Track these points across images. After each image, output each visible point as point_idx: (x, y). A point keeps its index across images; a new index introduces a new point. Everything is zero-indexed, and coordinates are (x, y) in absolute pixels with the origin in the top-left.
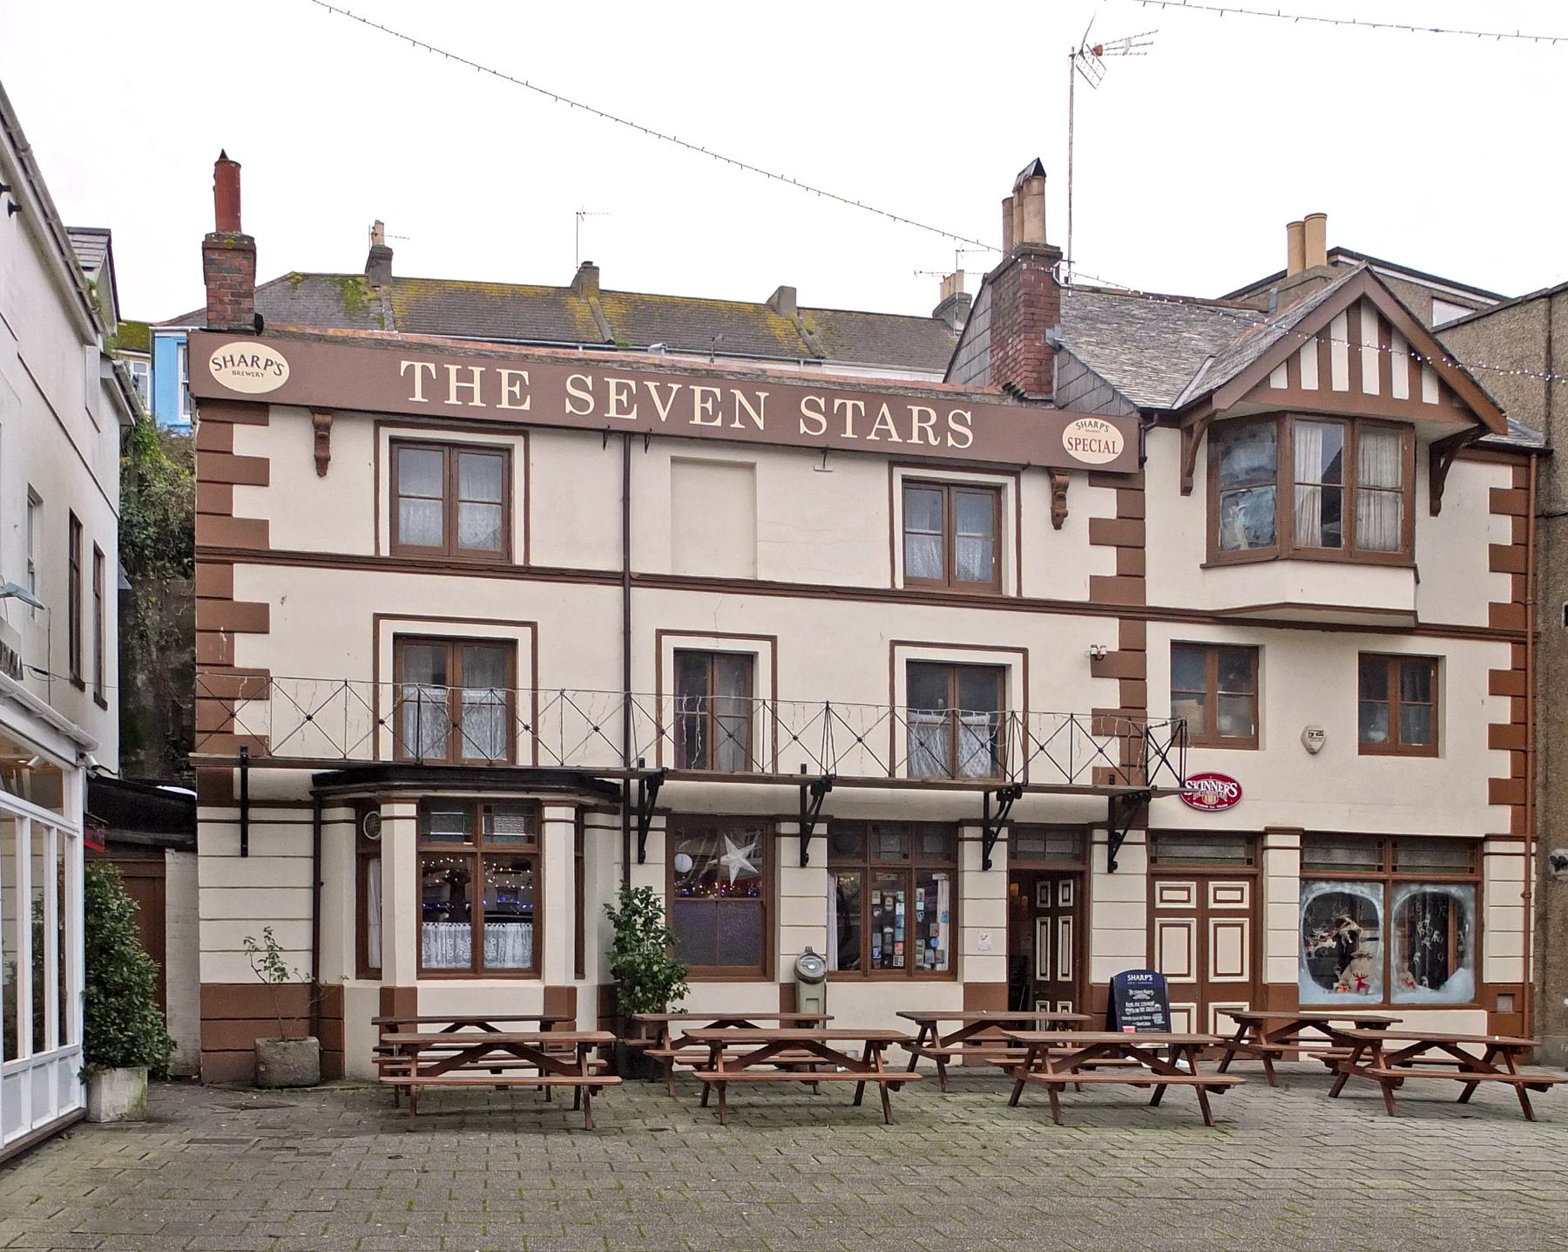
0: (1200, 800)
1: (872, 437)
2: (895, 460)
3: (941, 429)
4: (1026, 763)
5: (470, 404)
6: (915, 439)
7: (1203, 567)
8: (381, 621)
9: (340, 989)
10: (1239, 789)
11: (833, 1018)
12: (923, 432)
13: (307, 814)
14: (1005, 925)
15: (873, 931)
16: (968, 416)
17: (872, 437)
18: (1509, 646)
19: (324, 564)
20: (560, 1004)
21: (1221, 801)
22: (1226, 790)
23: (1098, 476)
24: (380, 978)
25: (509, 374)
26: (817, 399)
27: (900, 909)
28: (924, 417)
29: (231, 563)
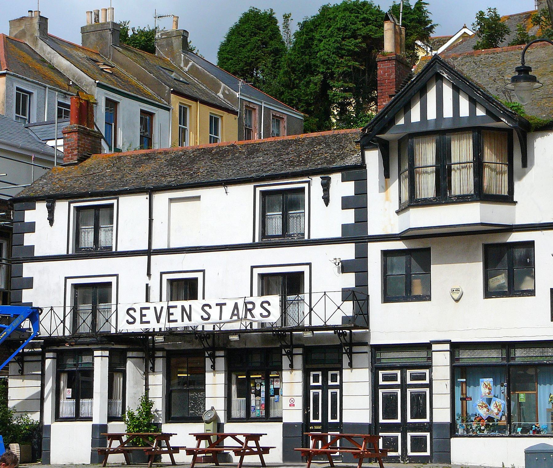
7: (398, 212)
8: (254, 269)
13: (39, 358)
14: (449, 393)
19: (45, 260)
24: (92, 421)
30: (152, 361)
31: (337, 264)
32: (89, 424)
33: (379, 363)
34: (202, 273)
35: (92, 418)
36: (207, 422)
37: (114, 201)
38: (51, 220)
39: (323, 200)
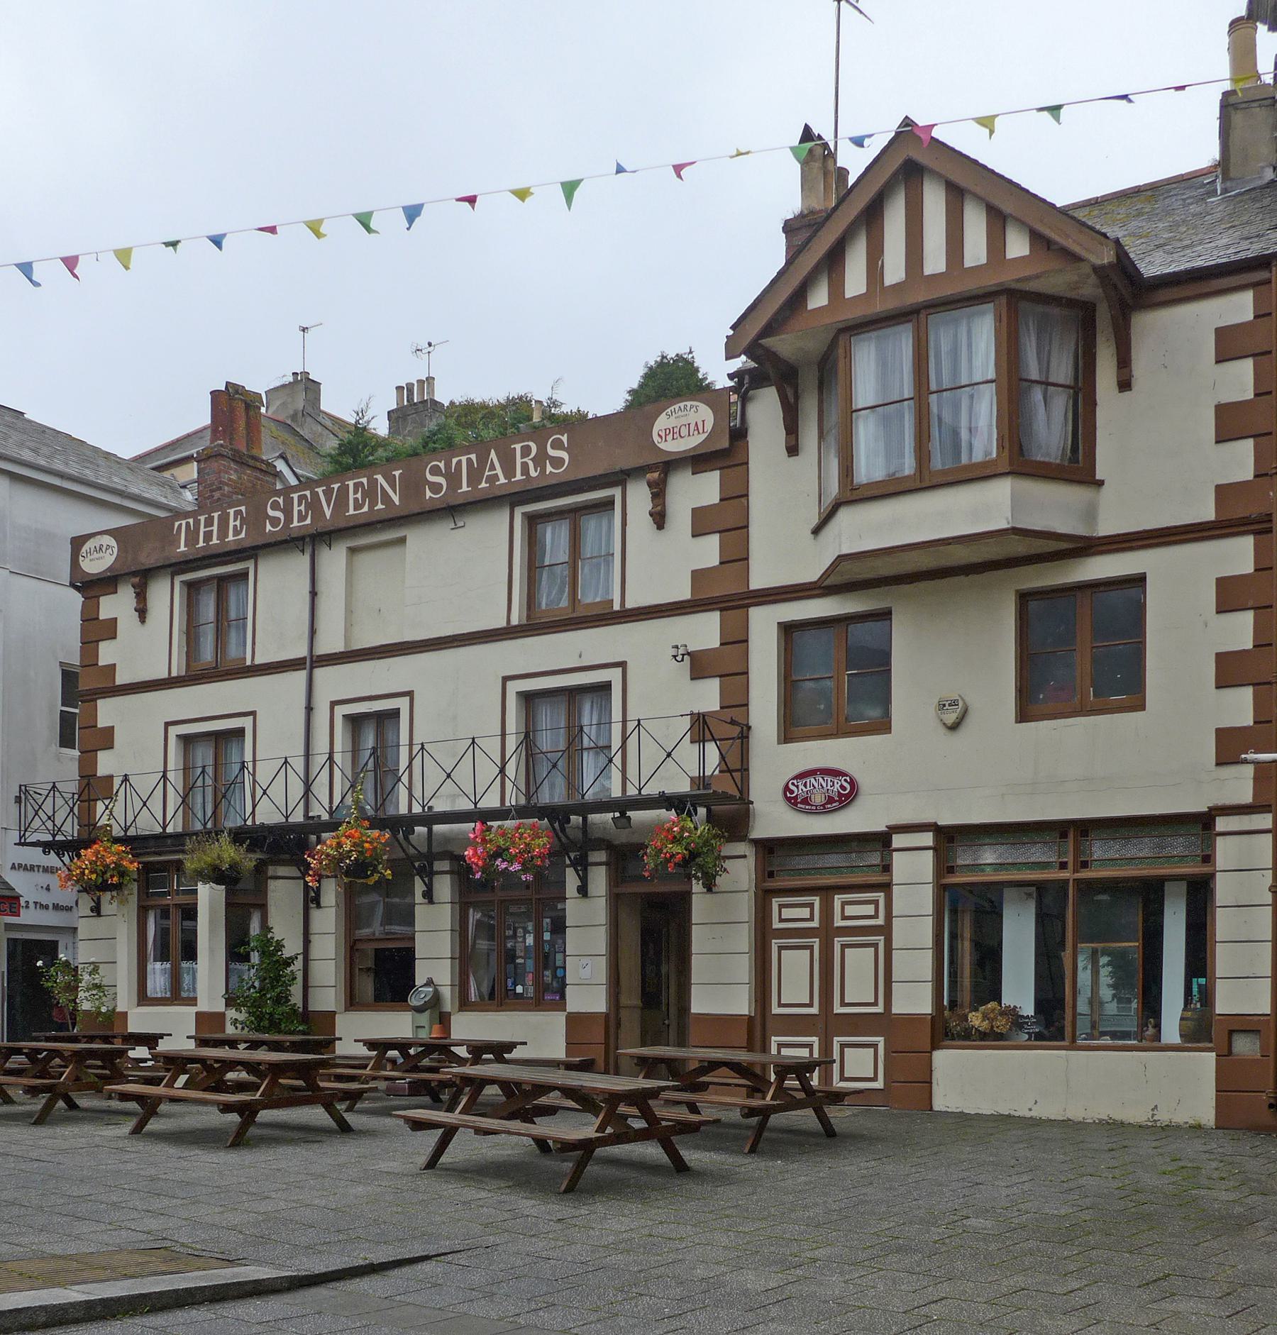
0: (806, 801)
1: (483, 485)
2: (514, 499)
3: (540, 460)
4: (254, 807)
5: (497, 483)
6: (519, 477)
9: (125, 1014)
10: (853, 783)
11: (340, 1039)
12: (525, 467)
15: (506, 963)
16: (565, 438)
17: (483, 485)
18: (718, 613)
20: (208, 1026)
21: (830, 800)
22: (837, 786)
23: (699, 461)
24: (196, 1005)
25: (355, 484)
26: (438, 463)
27: (547, 936)
28: (525, 452)
29: (95, 700)
30: (580, 872)
31: (679, 658)
32: (192, 1010)
33: (984, 876)
34: (621, 669)
35: (195, 999)
36: (419, 1010)
37: (616, 492)
38: (142, 613)
39: (137, 613)
